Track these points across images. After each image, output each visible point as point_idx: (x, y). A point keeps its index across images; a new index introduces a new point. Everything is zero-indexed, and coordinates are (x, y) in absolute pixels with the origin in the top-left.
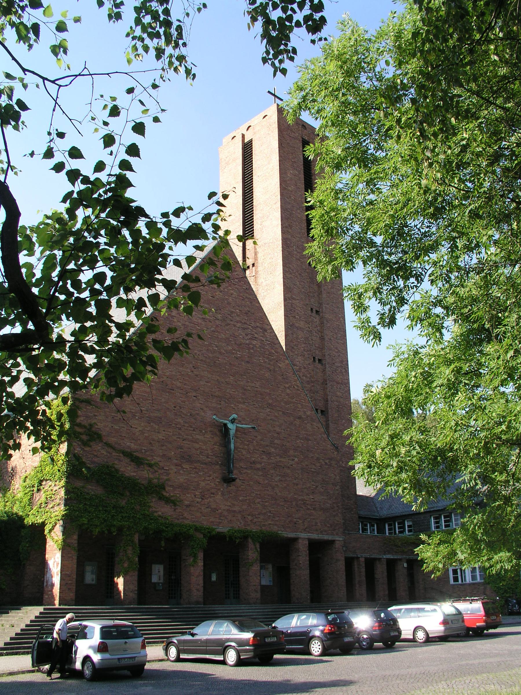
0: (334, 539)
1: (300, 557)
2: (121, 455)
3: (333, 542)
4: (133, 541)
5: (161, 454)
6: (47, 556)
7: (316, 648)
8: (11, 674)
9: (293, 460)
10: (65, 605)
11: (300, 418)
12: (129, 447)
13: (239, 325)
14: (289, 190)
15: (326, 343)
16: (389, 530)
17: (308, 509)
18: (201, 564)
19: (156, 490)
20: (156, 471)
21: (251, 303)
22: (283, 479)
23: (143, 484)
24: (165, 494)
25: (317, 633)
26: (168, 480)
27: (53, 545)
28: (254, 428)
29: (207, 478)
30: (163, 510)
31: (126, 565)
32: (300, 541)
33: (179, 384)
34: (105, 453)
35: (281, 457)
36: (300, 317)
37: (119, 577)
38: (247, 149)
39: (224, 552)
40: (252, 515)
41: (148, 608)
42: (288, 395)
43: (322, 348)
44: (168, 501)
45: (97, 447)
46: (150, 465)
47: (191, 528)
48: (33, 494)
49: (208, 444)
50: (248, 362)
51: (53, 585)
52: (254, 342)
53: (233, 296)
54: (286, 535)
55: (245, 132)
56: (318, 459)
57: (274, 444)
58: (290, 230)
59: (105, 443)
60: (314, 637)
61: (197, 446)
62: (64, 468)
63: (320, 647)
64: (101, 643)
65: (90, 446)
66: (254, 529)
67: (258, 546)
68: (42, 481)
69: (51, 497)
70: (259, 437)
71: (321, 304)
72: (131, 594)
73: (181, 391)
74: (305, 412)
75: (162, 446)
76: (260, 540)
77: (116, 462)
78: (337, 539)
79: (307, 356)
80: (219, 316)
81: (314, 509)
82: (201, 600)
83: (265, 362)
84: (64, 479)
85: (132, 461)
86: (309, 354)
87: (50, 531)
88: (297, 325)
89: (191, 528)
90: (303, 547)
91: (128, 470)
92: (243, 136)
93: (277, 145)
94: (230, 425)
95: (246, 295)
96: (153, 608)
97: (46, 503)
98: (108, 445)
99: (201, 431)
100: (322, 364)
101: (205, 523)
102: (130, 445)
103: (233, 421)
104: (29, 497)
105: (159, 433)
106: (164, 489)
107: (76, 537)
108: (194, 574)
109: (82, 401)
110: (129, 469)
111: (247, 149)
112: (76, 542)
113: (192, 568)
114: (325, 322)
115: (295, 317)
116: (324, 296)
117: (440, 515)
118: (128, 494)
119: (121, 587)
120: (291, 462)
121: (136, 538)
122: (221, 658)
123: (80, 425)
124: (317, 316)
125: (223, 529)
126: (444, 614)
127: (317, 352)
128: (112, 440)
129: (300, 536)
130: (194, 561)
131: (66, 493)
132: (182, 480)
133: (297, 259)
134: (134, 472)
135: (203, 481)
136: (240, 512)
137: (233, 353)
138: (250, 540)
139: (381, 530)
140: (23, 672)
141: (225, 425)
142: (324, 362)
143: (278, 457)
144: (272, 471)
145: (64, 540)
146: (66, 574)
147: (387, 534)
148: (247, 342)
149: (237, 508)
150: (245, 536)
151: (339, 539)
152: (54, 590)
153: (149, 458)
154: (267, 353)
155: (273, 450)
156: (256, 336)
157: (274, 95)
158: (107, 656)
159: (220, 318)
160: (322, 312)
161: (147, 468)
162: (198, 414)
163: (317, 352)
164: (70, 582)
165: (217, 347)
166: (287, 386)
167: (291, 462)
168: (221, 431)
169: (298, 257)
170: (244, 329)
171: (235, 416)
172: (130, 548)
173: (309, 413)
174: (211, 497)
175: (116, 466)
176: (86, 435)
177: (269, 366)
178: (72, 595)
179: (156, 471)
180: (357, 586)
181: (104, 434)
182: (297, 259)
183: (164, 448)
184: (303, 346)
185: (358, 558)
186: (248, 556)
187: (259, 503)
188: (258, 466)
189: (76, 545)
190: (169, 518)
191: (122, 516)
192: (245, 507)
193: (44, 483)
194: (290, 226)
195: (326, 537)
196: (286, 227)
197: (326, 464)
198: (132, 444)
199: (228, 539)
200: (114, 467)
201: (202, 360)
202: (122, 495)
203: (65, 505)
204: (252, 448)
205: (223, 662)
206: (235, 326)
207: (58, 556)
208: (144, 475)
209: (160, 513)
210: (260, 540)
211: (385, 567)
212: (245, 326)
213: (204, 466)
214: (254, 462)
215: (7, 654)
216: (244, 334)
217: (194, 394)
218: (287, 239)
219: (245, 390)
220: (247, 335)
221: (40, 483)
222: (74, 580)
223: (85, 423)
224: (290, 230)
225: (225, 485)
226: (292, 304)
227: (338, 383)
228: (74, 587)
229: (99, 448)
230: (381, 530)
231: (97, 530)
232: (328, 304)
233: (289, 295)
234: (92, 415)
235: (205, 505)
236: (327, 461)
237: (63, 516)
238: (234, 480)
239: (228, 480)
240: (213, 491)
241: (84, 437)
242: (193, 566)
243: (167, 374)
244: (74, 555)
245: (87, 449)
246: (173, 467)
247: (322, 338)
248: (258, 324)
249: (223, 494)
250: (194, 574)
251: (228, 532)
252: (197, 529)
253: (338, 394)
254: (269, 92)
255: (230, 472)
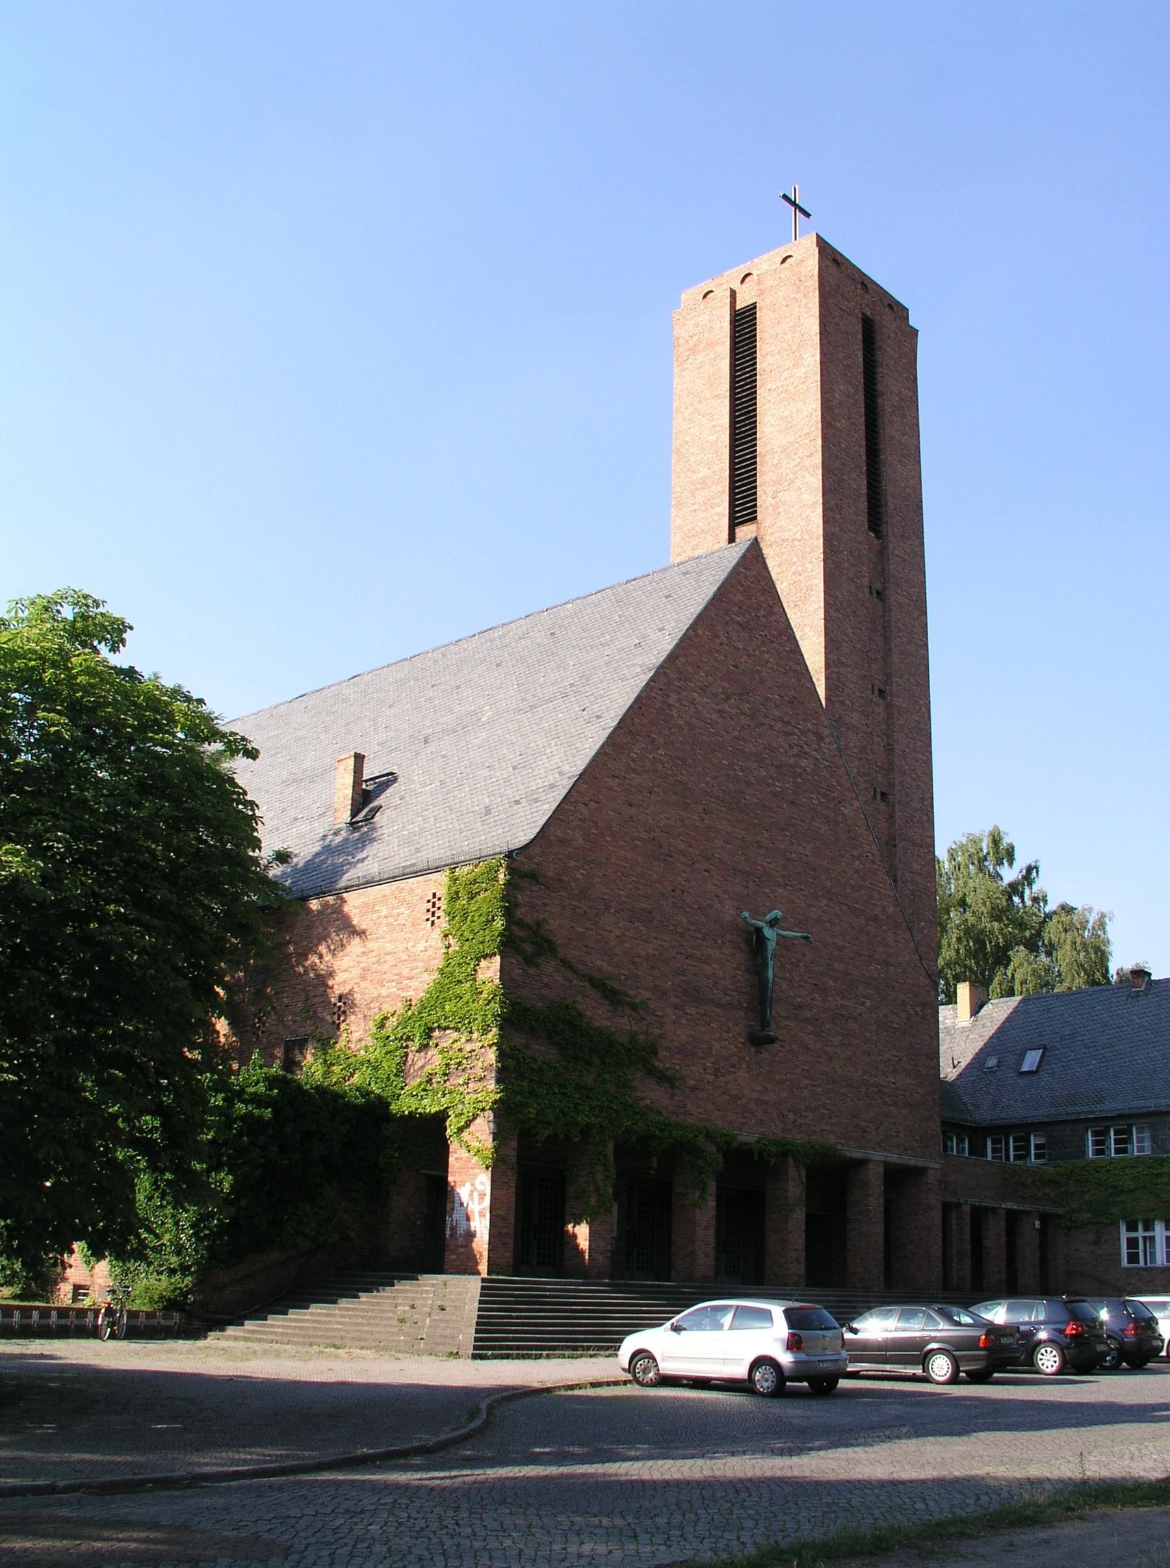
0: (925, 1164)
1: (871, 1199)
2: (587, 984)
3: (920, 1171)
4: (605, 1156)
5: (651, 985)
6: (450, 1179)
7: (1048, 1360)
8: (595, 1385)
9: (863, 1004)
10: (498, 1274)
11: (876, 919)
12: (600, 969)
13: (778, 726)
14: (837, 429)
15: (897, 762)
16: (994, 1150)
17: (885, 1103)
18: (712, 1203)
19: (641, 1055)
20: (643, 1019)
21: (799, 680)
22: (846, 1042)
23: (622, 1045)
24: (657, 1064)
25: (1043, 1335)
26: (661, 1036)
27: (469, 1160)
28: (806, 938)
29: (725, 1035)
30: (653, 1095)
31: (593, 1202)
32: (871, 1166)
33: (680, 845)
34: (561, 980)
35: (844, 998)
36: (853, 703)
37: (577, 1222)
38: (744, 325)
39: (746, 1179)
40: (795, 1112)
41: (659, 1286)
42: (857, 871)
43: (889, 770)
44: (666, 1079)
45: (549, 967)
46: (633, 1007)
47: (700, 1132)
48: (406, 1055)
49: (724, 966)
50: (793, 803)
51: (471, 1235)
52: (804, 763)
53: (769, 665)
54: (848, 1154)
55: (736, 285)
56: (903, 1003)
57: (834, 970)
58: (838, 516)
59: (561, 961)
60: (1040, 1342)
61: (708, 970)
62: (496, 1007)
63: (1057, 1359)
64: (792, 1335)
65: (537, 966)
66: (798, 1137)
67: (803, 1173)
68: (431, 1030)
69: (459, 1064)
70: (809, 957)
71: (889, 676)
72: (601, 1258)
73: (683, 859)
74: (884, 910)
75: (653, 968)
76: (808, 1162)
77: (579, 999)
78: (931, 1165)
79: (863, 785)
80: (746, 707)
81: (895, 1104)
82: (711, 1274)
83: (820, 803)
84: (495, 1030)
85: (605, 997)
86: (866, 782)
87: (460, 1130)
88: (848, 719)
89: (700, 1132)
90: (874, 1176)
91: (597, 1014)
92: (733, 294)
93: (816, 328)
94: (768, 932)
95: (791, 663)
96: (663, 1286)
97: (445, 1074)
98: (565, 963)
99: (716, 941)
100: (888, 804)
101: (720, 1123)
102: (599, 964)
103: (773, 923)
104: (397, 1060)
105: (647, 941)
106: (655, 1053)
107: (514, 1144)
108: (700, 1224)
109: (526, 876)
110: (600, 1012)
111: (744, 325)
112: (514, 1153)
113: (698, 1211)
114: (896, 714)
115: (842, 702)
116: (895, 659)
117: (1130, 1126)
118: (597, 1062)
119: (583, 1242)
120: (861, 1009)
121: (610, 1148)
122: (918, 1371)
123: (520, 924)
124: (881, 701)
125: (748, 1137)
126: (781, 1340)
127: (880, 778)
128: (572, 954)
129: (871, 1157)
130: (702, 1197)
131: (501, 1056)
132: (683, 1037)
133: (849, 579)
134: (608, 1018)
135: (719, 1039)
136: (775, 1104)
137: (769, 785)
138: (791, 1162)
139: (977, 1150)
140: (608, 1384)
141: (759, 930)
142: (890, 797)
143: (838, 998)
144: (828, 1026)
145: (497, 1149)
146: (499, 1216)
147: (989, 1158)
148: (792, 761)
149: (770, 1097)
150: (785, 1152)
151: (934, 1165)
152: (474, 1245)
153: (632, 993)
154: (824, 785)
155: (831, 983)
156: (806, 749)
157: (794, 204)
158: (803, 1356)
159: (747, 711)
160: (891, 694)
161: (629, 1012)
162: (710, 906)
163: (880, 778)
164: (505, 1231)
165: (742, 770)
166: (856, 853)
167: (861, 1009)
168: (748, 941)
169: (851, 575)
170: (787, 734)
171: (777, 913)
172: (599, 1168)
173: (891, 910)
174: (729, 1073)
175: (578, 1006)
176: (532, 943)
177: (826, 812)
178: (508, 1256)
179: (643, 1019)
180: (955, 1260)
181: (559, 941)
182: (849, 579)
183: (656, 972)
184: (856, 763)
185: (959, 1205)
186: (787, 1191)
187: (806, 1088)
188: (808, 1014)
189: (514, 1160)
190: (664, 1111)
191: (590, 1106)
192: (784, 1095)
193: (436, 1033)
194: (839, 508)
195: (913, 1161)
196: (832, 510)
197: (917, 1014)
198: (604, 964)
199: (756, 1157)
200: (576, 1009)
201: (717, 798)
202: (589, 1063)
203: (498, 1082)
204: (797, 978)
205: (926, 1380)
206: (771, 727)
207: (484, 1181)
208: (622, 1024)
209: (648, 1102)
210: (808, 1162)
211: (1003, 1224)
212: (789, 729)
213: (719, 1011)
214: (800, 1007)
215: (518, 1357)
216: (786, 745)
217: (706, 866)
218: (833, 534)
219: (789, 860)
220: (791, 747)
221: (428, 1032)
222: (512, 1227)
223: (528, 919)
224: (838, 516)
225: (753, 1049)
226: (839, 673)
227: (915, 844)
228: (512, 1241)
229: (552, 969)
230: (977, 1150)
231: (547, 1132)
232: (901, 677)
233: (833, 657)
234: (539, 903)
235: (721, 1091)
236: (918, 1009)
237: (495, 1102)
238: (772, 1040)
239: (759, 1040)
240: (734, 1060)
241: (528, 948)
242: (699, 1206)
243: (662, 824)
244: (512, 1178)
245: (532, 971)
246: (669, 1011)
247: (889, 749)
248: (810, 726)
249: (749, 1068)
250: (700, 1224)
251: (758, 1142)
252: (709, 1136)
253: (915, 866)
254: (808, 215)
255: (765, 1024)
